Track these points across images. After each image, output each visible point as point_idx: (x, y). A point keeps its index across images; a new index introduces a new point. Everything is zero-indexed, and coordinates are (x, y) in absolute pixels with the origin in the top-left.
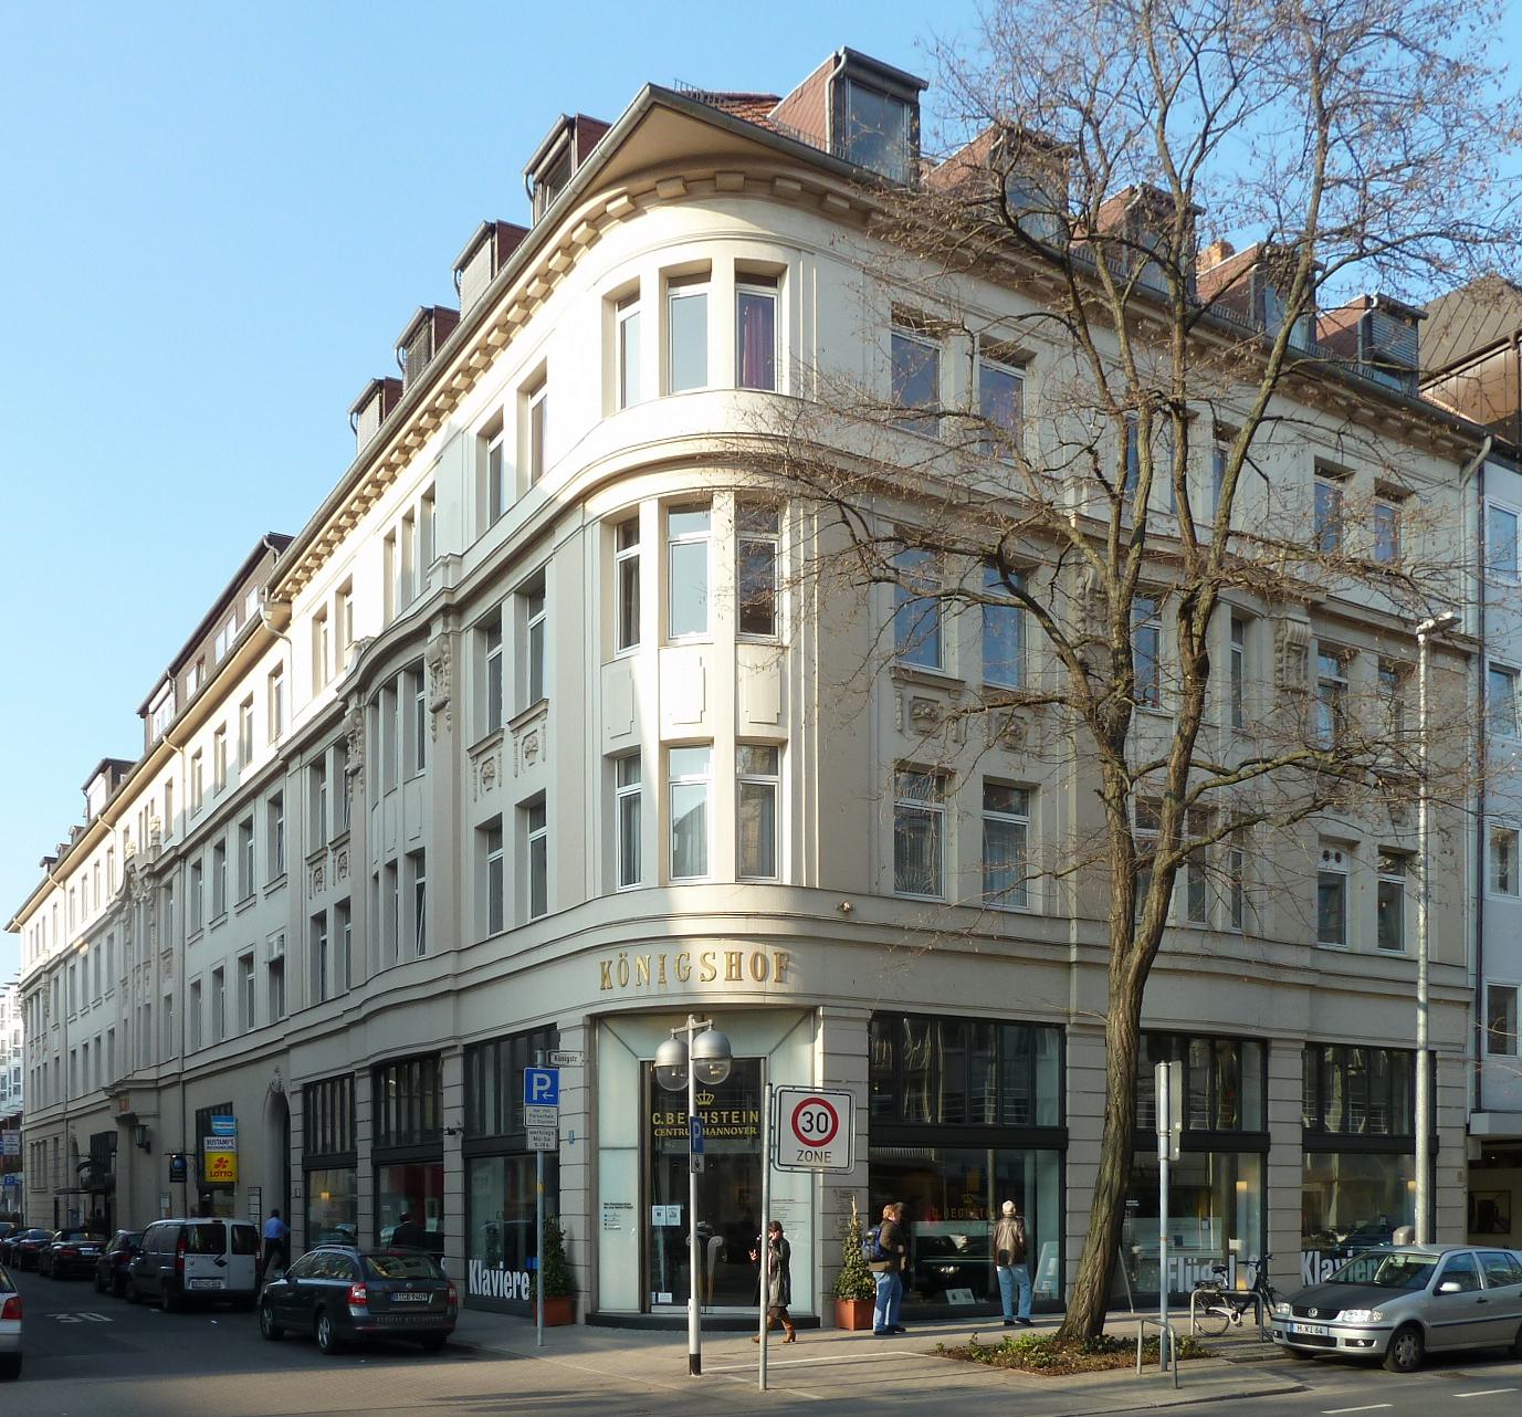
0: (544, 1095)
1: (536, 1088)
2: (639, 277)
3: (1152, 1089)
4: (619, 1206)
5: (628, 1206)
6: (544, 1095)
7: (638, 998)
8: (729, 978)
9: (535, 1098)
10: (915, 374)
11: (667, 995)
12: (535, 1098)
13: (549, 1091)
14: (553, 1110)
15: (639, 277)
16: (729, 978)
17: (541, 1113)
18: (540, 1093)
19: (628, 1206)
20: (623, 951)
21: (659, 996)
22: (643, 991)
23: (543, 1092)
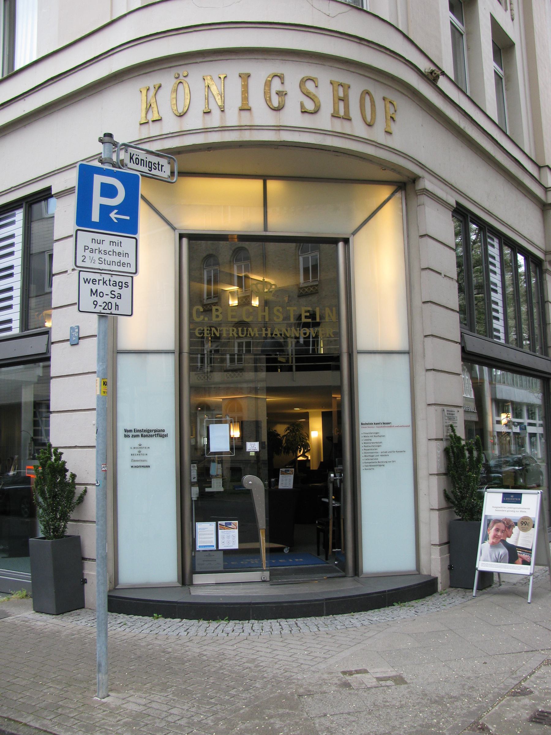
0: (113, 215)
1: (98, 200)
2: (51, 186)
3: (191, 344)
4: (146, 433)
5: (160, 434)
6: (113, 215)
7: (206, 130)
8: (335, 116)
9: (95, 217)
10: (123, 149)
11: (251, 128)
12: (95, 217)
13: (121, 209)
14: (127, 244)
15: (51, 186)
16: (335, 116)
17: (106, 246)
18: (105, 210)
19: (160, 434)
20: (183, 71)
21: (240, 128)
22: (215, 120)
23: (110, 209)
